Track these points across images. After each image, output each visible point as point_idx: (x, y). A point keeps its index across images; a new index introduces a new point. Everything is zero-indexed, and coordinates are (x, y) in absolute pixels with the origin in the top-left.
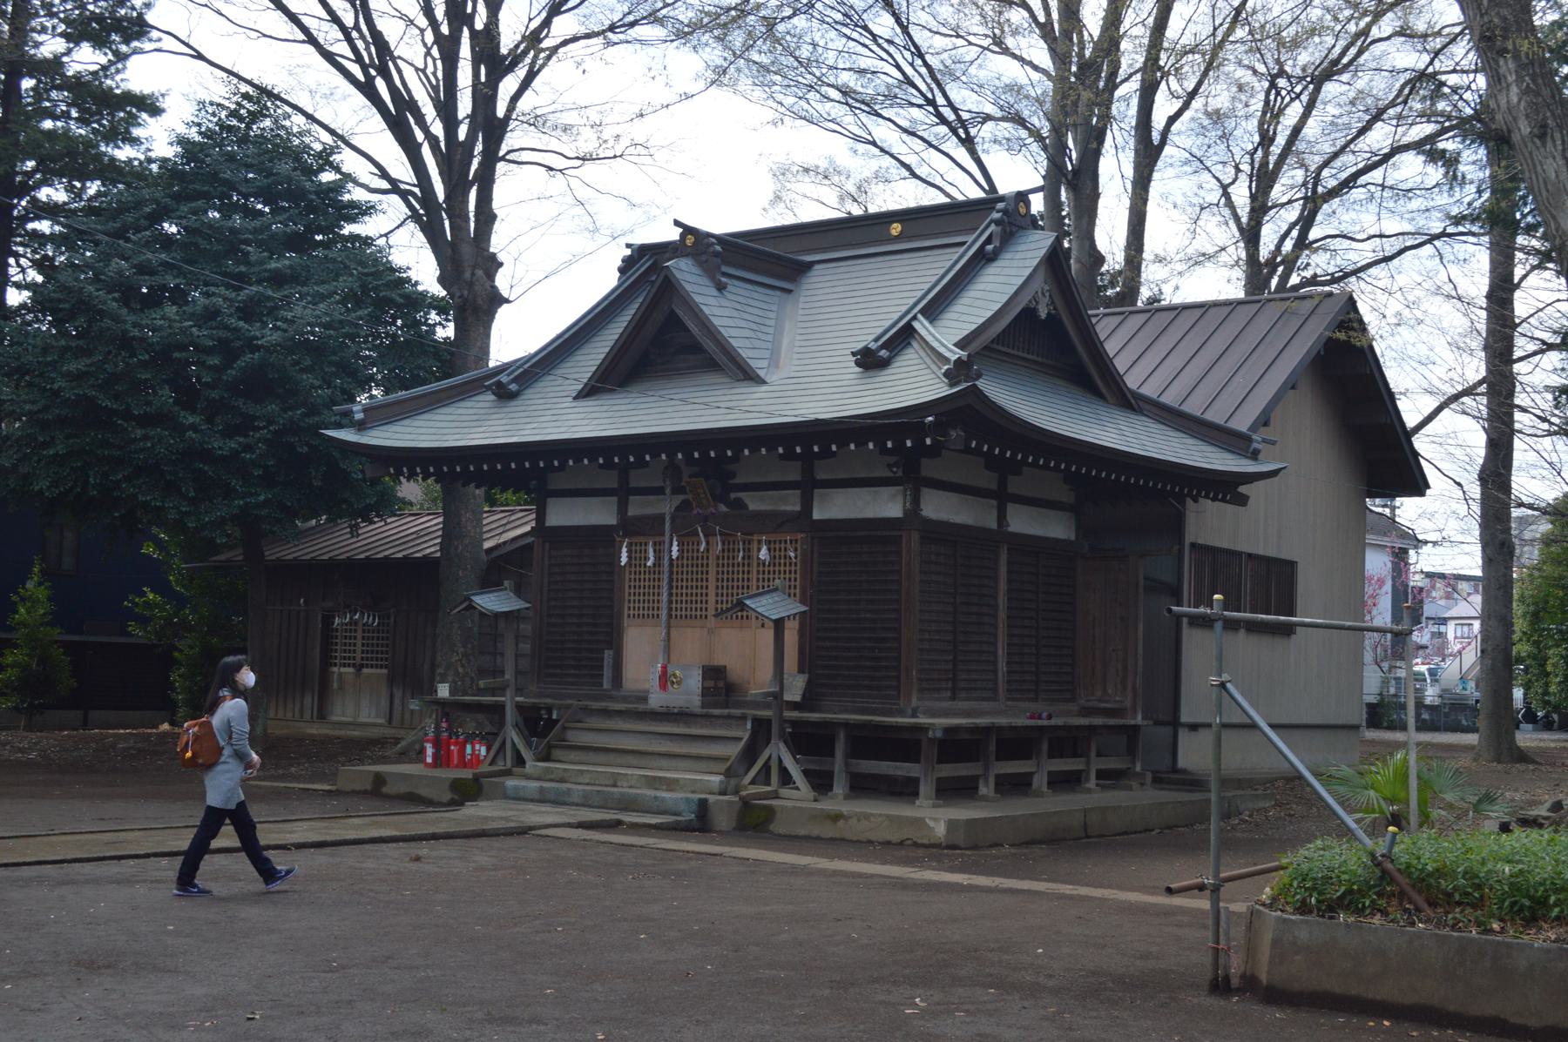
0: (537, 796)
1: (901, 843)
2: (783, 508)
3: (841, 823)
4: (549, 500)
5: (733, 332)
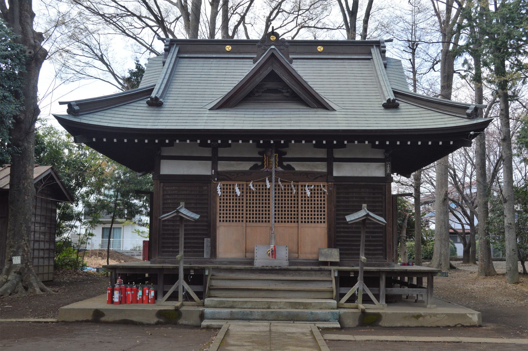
0: (229, 317)
1: (455, 326)
2: (316, 170)
3: (421, 319)
4: (162, 161)
5: (317, 89)
